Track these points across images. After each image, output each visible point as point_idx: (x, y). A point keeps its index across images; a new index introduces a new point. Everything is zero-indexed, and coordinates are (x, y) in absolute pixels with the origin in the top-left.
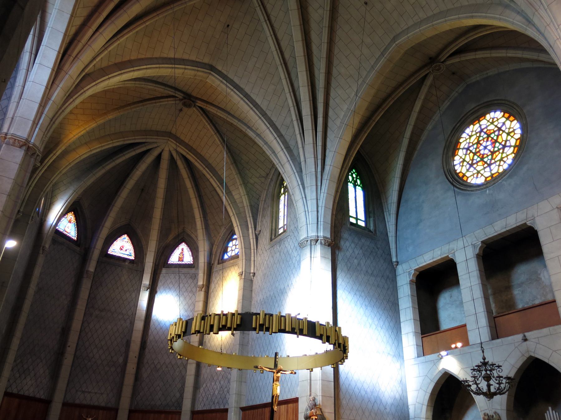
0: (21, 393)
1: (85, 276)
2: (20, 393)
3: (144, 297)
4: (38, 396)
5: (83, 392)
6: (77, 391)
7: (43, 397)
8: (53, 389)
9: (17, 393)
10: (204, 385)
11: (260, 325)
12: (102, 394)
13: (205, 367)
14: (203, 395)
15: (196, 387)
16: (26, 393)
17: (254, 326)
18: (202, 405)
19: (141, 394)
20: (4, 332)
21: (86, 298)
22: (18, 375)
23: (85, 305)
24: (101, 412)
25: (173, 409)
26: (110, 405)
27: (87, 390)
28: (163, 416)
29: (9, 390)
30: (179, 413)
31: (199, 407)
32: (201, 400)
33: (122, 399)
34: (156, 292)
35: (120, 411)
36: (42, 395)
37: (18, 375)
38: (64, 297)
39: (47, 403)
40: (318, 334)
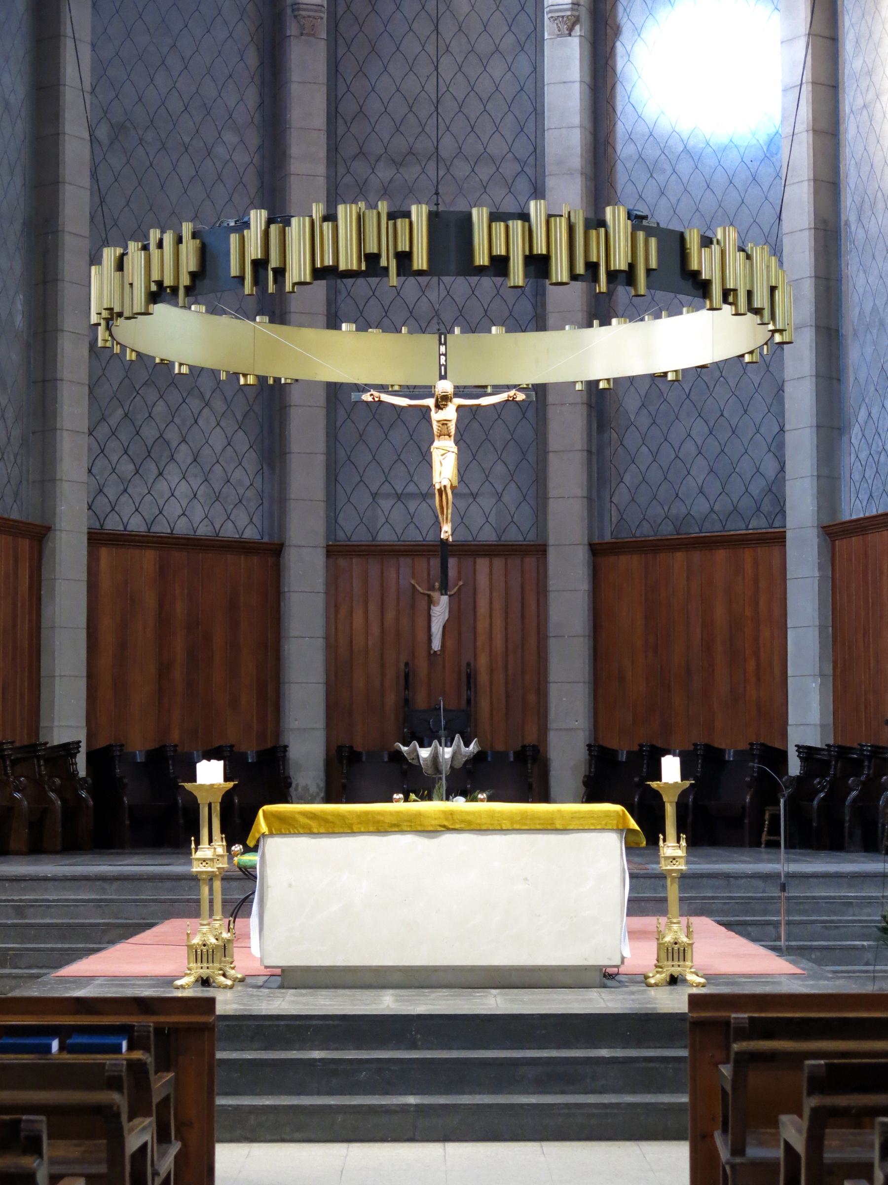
0: (162, 528)
1: (292, 29)
2: (156, 529)
3: (564, 61)
4: (229, 532)
5: (399, 497)
6: (374, 496)
7: (250, 534)
8: (276, 502)
9: (143, 528)
10: (863, 415)
11: (256, 263)
12: (474, 496)
13: (855, 334)
14: (863, 455)
15: (832, 423)
16: (182, 528)
17: (234, 271)
18: (864, 496)
19: (627, 478)
20: (19, 320)
21: (320, 120)
22: (127, 468)
23: (322, 153)
24: (483, 564)
25: (758, 524)
26: (513, 536)
27: (411, 488)
28: (721, 555)
29: (113, 524)
30: (779, 539)
31: (854, 508)
32: (856, 476)
33: (553, 506)
34: (617, 31)
35: (552, 556)
36: (243, 525)
37: (131, 467)
38: (230, 138)
39: (271, 553)
40: (482, 258)
